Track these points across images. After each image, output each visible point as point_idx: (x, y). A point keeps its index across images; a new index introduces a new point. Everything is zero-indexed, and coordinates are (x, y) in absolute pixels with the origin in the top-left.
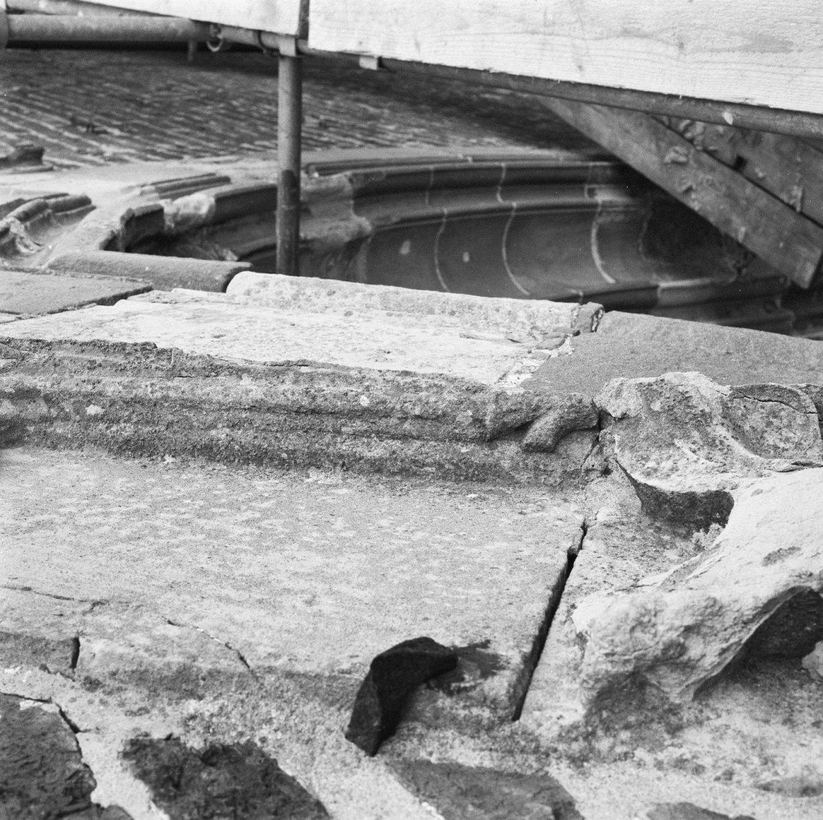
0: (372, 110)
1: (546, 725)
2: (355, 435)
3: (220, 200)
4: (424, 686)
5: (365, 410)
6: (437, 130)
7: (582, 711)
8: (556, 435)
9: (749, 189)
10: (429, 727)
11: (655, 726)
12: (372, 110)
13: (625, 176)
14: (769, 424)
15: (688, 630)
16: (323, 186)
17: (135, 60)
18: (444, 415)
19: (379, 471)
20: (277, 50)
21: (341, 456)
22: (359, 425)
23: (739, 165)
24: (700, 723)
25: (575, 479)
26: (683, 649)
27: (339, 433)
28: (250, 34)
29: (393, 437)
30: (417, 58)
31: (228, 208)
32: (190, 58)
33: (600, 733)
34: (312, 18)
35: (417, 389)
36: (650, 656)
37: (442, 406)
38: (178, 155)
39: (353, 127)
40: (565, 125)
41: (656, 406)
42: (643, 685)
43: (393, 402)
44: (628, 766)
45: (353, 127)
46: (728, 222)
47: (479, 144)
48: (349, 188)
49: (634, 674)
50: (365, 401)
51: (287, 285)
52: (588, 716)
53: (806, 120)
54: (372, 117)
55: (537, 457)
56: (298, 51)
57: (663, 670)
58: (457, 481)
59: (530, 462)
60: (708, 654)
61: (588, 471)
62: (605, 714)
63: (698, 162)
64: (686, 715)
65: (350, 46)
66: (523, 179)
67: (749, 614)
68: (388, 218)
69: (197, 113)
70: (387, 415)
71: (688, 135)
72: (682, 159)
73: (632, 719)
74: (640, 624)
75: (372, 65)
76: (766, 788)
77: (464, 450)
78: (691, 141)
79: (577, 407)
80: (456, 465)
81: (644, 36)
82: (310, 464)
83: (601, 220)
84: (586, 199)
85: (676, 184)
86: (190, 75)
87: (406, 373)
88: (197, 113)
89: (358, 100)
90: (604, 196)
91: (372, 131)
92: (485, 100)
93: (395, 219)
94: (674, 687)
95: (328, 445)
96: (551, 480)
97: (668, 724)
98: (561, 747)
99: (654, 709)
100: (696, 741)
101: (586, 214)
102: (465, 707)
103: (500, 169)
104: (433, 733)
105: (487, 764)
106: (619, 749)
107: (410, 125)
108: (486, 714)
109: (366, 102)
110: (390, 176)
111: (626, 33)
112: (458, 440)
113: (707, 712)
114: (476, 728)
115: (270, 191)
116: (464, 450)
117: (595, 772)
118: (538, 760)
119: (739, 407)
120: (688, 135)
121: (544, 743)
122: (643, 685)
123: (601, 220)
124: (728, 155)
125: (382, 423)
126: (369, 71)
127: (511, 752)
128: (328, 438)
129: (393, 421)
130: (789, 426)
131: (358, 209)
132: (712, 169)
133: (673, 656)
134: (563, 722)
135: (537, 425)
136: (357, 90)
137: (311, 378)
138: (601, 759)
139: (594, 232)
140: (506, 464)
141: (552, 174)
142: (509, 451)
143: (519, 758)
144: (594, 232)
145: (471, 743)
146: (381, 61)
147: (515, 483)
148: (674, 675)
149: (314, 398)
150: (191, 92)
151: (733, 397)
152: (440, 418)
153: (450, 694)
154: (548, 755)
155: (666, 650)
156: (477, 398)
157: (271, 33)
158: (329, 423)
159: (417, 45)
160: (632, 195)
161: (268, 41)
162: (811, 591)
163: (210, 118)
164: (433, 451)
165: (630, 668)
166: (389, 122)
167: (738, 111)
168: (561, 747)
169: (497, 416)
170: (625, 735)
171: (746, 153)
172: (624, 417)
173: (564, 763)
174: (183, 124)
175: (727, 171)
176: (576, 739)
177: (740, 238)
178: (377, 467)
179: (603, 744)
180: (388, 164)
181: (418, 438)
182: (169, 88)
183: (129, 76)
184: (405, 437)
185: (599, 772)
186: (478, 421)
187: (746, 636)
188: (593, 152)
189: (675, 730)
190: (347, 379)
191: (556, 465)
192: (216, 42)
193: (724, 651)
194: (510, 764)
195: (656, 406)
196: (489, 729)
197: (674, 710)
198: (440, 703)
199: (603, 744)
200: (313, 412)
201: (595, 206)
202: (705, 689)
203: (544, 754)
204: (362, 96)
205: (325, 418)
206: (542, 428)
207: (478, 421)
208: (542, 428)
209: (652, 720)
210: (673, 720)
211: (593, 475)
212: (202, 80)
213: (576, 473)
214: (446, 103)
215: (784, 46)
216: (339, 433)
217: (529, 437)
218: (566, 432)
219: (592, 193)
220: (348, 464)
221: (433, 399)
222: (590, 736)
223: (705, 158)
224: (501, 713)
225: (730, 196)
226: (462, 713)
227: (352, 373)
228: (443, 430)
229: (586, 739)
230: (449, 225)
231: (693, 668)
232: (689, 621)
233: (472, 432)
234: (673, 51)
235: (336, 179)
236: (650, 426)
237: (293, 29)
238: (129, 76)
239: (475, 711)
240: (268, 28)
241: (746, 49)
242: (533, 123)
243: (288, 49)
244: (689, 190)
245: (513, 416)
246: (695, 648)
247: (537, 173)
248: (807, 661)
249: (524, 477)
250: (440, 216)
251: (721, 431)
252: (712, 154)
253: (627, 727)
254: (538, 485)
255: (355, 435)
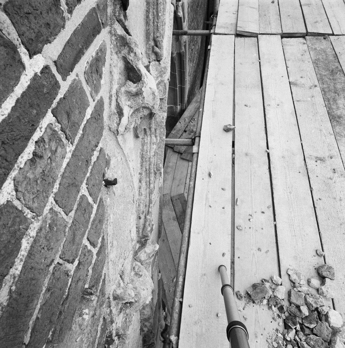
0: (195, 62)
1: (116, 26)
2: (153, 12)
3: (181, 18)
4: (121, 2)
5: (158, 15)
6: (191, 75)
7: (119, 34)
8: (156, 52)
9: (181, 133)
10: (113, 3)
11: (117, 49)
12: (195, 62)
13: (182, 111)
14: (160, 90)
15: (135, 53)
16: (182, 45)
17: (205, 9)
18: (158, 30)
19: (147, 17)
20: (212, 29)
21: (149, 9)
22: (155, 13)
23: (185, 131)
24: (118, 58)
25: (148, 57)
26: (132, 52)
27: (154, 9)
28: (215, 24)
29: (153, 20)
30: (211, 56)
31: (179, 20)
32: (206, 22)
33: (115, 37)
34: (218, 36)
35: (162, 26)
36: (131, 45)
37: (160, 30)
38: (189, 14)
39: (192, 56)
40: (192, 99)
41: (162, 69)
42: (125, 46)
43: (160, 20)
44: (110, 43)
45: (192, 56)
46: (175, 130)
47: (188, 83)
48: (182, 51)
49: (127, 43)
50: (160, 14)
51: (172, 17)
52: (118, 35)
53: (201, 122)
54: (193, 62)
55: (152, 49)
56: (211, 33)
57: (128, 49)
58: (146, 33)
59: (150, 47)
60: (131, 57)
61: (149, 58)
62: (119, 38)
63: (185, 124)
64: (119, 55)
65: (213, 43)
66: (182, 90)
67: (138, 67)
68: (175, 60)
69: (195, 20)
70: (157, 19)
71: (190, 122)
72: (186, 121)
73: (118, 44)
74: (136, 44)
75: (209, 48)
76: (110, 65)
77: (152, 35)
78: (189, 123)
79: (161, 56)
80: (149, 33)
81: (215, 95)
82: (147, 3)
83: (174, 107)
84: (178, 104)
85: (181, 120)
86: (202, 21)
87: (165, 24)
88: (195, 20)
89: (196, 59)
90: (179, 107)
91: (191, 61)
92: (195, 87)
93: (175, 62)
94: (125, 51)
95: (151, 7)
96: (147, 51)
97: (117, 52)
98: (113, 29)
99: (120, 48)
100: (115, 57)
101: (175, 104)
102: (118, 10)
103: (184, 86)
104: (112, 4)
105: (108, 14)
106: (113, 41)
107: (192, 69)
108: (117, 14)
109: (196, 61)
110: (184, 61)
111: (215, 92)
112: (154, 33)
113: (120, 59)
114: (114, 13)
115: (182, 29)
116: (152, 35)
117: (109, 35)
118: (110, 25)
119: (163, 84)
120: (190, 122)
121: (113, 26)
122: (125, 46)
123: (174, 107)
124: (187, 129)
125: (156, 18)
126: (208, 47)
127: (111, 19)
128: (152, 7)
129: (156, 20)
130: (160, 94)
131: (177, 53)
132: (184, 127)
133: (131, 50)
134: (117, 30)
135: (157, 48)
136: (198, 59)
137: (163, 4)
138: (111, 37)
139: (172, 105)
140: (150, 43)
141: (183, 95)
142: (152, 43)
143: (110, 21)
144: (172, 105)
145: (111, 11)
146: (210, 49)
147: (146, 44)
148: (127, 51)
149: (160, 4)
150: (199, 21)
151: (164, 83)
152: (158, 29)
153: (120, 8)
154: (111, 26)
155: (132, 48)
156: (161, 37)
157: (215, 27)
158: (155, 7)
159: (213, 56)
160: (179, 113)
161: (214, 27)
162: (141, 79)
163: (194, 24)
164: (151, 28)
165: (128, 42)
166: (193, 65)
167: (202, 111)
168: (113, 29)
169: (159, 41)
170: (115, 43)
171: (187, 132)
172: (160, 64)
173: (109, 29)
174: (193, 17)
175: (184, 129)
176: (114, 32)
177: (172, 132)
178: (148, 17)
179: (113, 38)
180: (186, 62)
181: (154, 25)
182: (200, 15)
183: (202, 6)
184: (154, 23)
185: (109, 36)
186: (157, 37)
187: (134, 66)
188: (187, 106)
189: (116, 53)
190: (164, 11)
191: (150, 52)
192: (213, 17)
193: (132, 60)
194: (109, 19)
195: (162, 69)
196: (114, 15)
197: (120, 52)
198: (118, 6)
199: (113, 38)
200: (157, 4)
201: (177, 105)
202: (125, 59)
203: (111, 25)
204: (197, 60)
205: (156, 6)
206: (157, 49)
207: (157, 37)
208: (157, 49)
209: (118, 48)
210: (118, 52)
211: (149, 59)
212: (201, 24)
213: (149, 56)
214: (195, 79)
215: (213, 117)
216: (154, 9)
217: (155, 47)
218: (156, 54)
219: (179, 105)
220: (148, 11)
221: (161, 28)
222: (115, 35)
223: (186, 125)
224: (118, 17)
225: (180, 130)
226: (117, 10)
227: (165, 13)
228: (155, 30)
229: (115, 34)
230: (174, 74)
231: (129, 54)
232: (137, 53)
233: (155, 36)
234: (212, 100)
235: (183, 48)
236: (159, 68)
237: (216, 32)
238: (202, 6)
239: (117, 12)
240: (216, 27)
241: (213, 111)
242: (191, 95)
243: (212, 31)
244: (180, 123)
245: (159, 44)
246: (132, 55)
247: (183, 93)
248: (128, 81)
249: (148, 46)
250: (176, 72)
251: (160, 79)
252: (187, 126)
253: (116, 43)
254: (146, 49)
255: (153, 12)
